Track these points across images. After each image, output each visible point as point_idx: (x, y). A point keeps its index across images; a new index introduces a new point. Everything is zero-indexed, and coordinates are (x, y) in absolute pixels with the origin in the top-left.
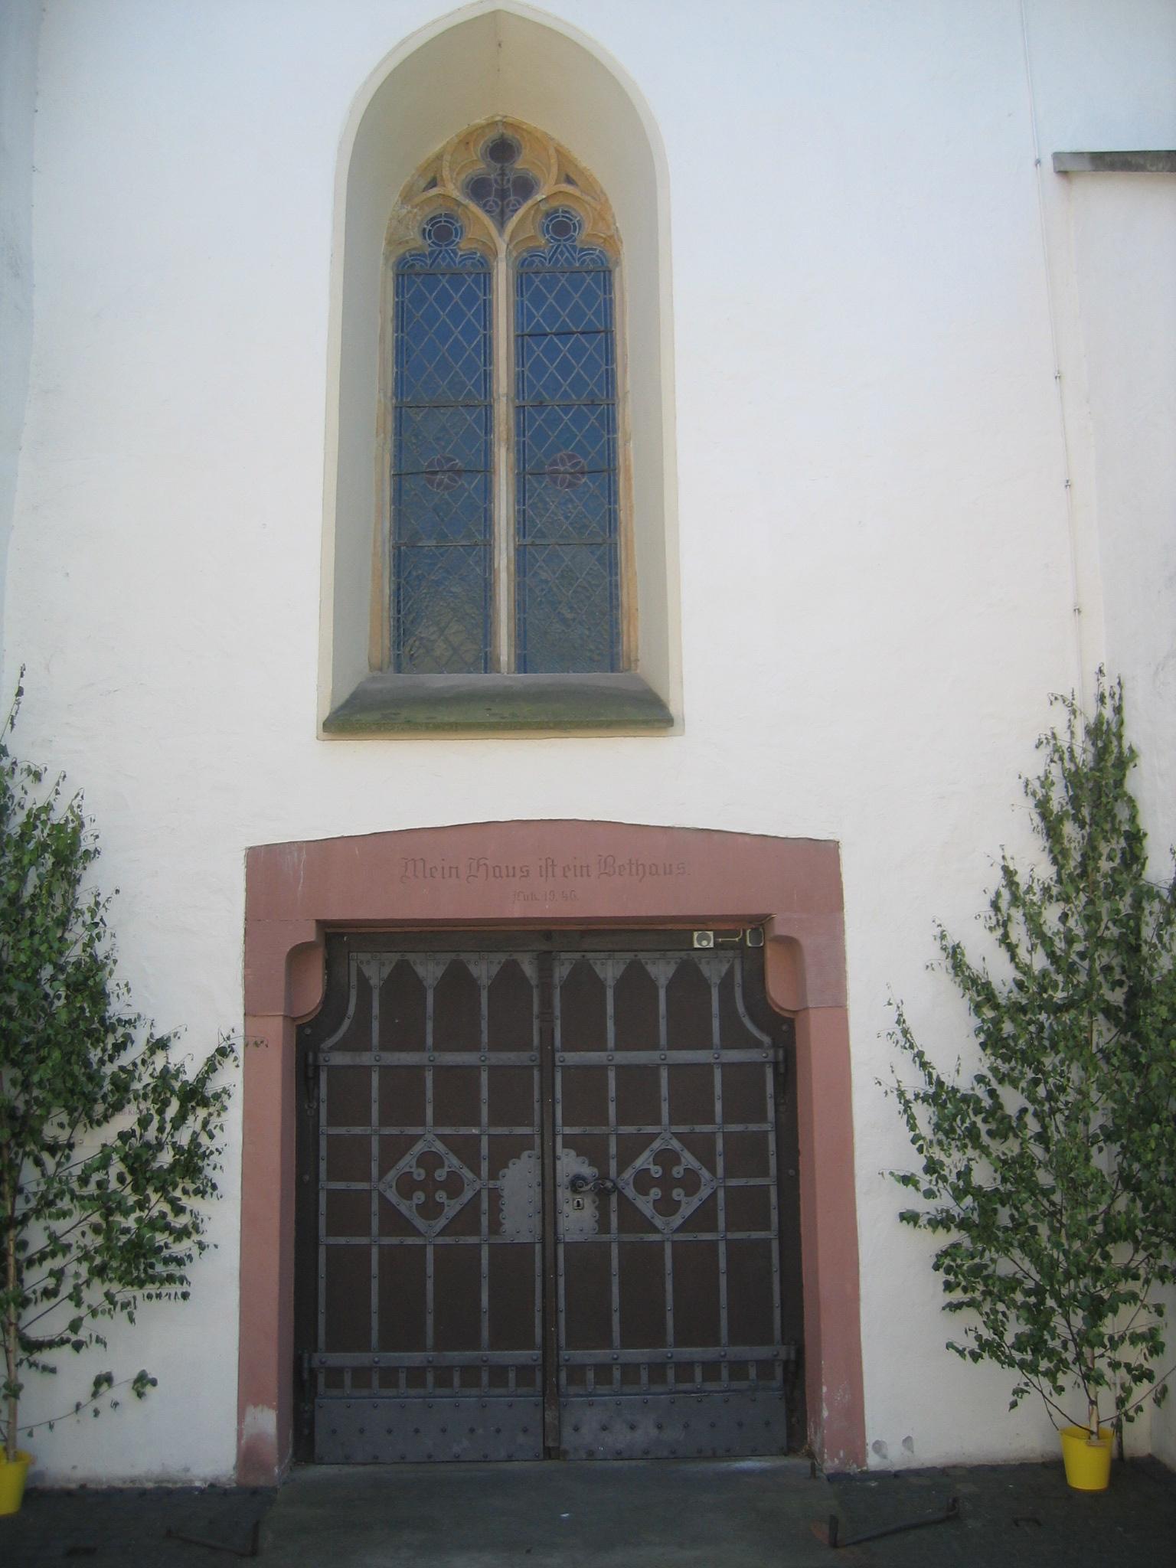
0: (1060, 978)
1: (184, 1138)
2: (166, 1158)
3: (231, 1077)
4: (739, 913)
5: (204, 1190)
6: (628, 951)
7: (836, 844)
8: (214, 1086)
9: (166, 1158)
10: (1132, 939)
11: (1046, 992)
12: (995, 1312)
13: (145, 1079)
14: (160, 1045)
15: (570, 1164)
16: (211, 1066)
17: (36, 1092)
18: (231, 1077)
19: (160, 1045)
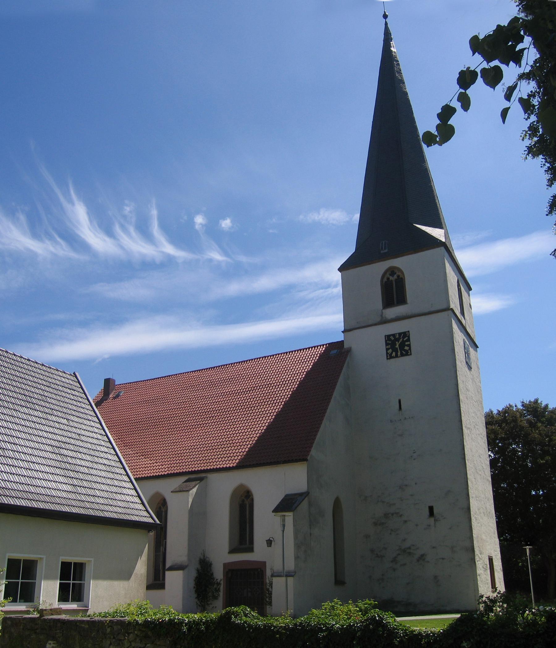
0: (367, 615)
1: (218, 587)
2: (217, 589)
3: (222, 582)
4: (391, 323)
5: (220, 591)
6: (305, 498)
7: (105, 379)
8: (221, 582)
9: (217, 589)
10: (481, 399)
11: (492, 611)
12: (240, 620)
13: (216, 582)
14: (217, 580)
15: (249, 590)
16: (220, 581)
17: (150, 617)
18: (222, 582)
19: (217, 580)
